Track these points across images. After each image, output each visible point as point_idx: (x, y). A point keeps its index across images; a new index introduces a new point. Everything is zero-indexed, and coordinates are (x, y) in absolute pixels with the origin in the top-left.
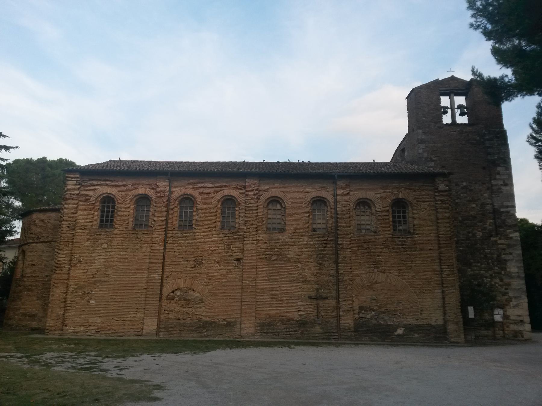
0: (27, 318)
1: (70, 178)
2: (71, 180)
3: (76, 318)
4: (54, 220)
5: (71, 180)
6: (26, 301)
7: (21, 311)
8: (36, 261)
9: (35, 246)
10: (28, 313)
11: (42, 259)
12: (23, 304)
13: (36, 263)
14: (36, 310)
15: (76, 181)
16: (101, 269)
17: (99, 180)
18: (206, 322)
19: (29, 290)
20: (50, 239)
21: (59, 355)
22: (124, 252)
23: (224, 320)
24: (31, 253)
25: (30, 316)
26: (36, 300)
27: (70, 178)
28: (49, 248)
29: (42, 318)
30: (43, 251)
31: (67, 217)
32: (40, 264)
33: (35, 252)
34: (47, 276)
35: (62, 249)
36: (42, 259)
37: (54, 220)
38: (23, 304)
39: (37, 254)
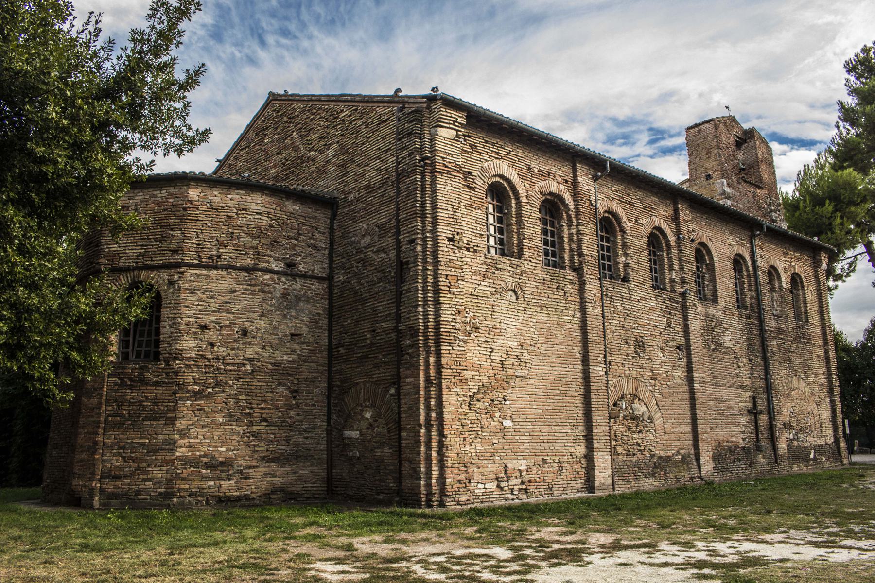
0: (204, 471)
1: (448, 122)
2: (447, 126)
3: (486, 462)
4: (257, 213)
5: (447, 126)
6: (192, 425)
7: (178, 454)
8: (213, 318)
9: (206, 275)
10: (205, 459)
11: (233, 313)
12: (184, 433)
13: (213, 322)
14: (228, 450)
15: (455, 132)
16: (515, 350)
17: (486, 142)
18: (660, 457)
19: (197, 395)
20: (249, 262)
21: (763, 542)
22: (544, 315)
23: (678, 453)
24: (192, 293)
25: (207, 466)
26: (223, 423)
27: (448, 122)
28: (251, 285)
29: (251, 470)
30: (233, 292)
31: (447, 216)
32: (226, 326)
33: (207, 291)
34: (250, 360)
35: (445, 292)
36: (233, 313)
37: (257, 213)
38: (184, 433)
39: (212, 298)
